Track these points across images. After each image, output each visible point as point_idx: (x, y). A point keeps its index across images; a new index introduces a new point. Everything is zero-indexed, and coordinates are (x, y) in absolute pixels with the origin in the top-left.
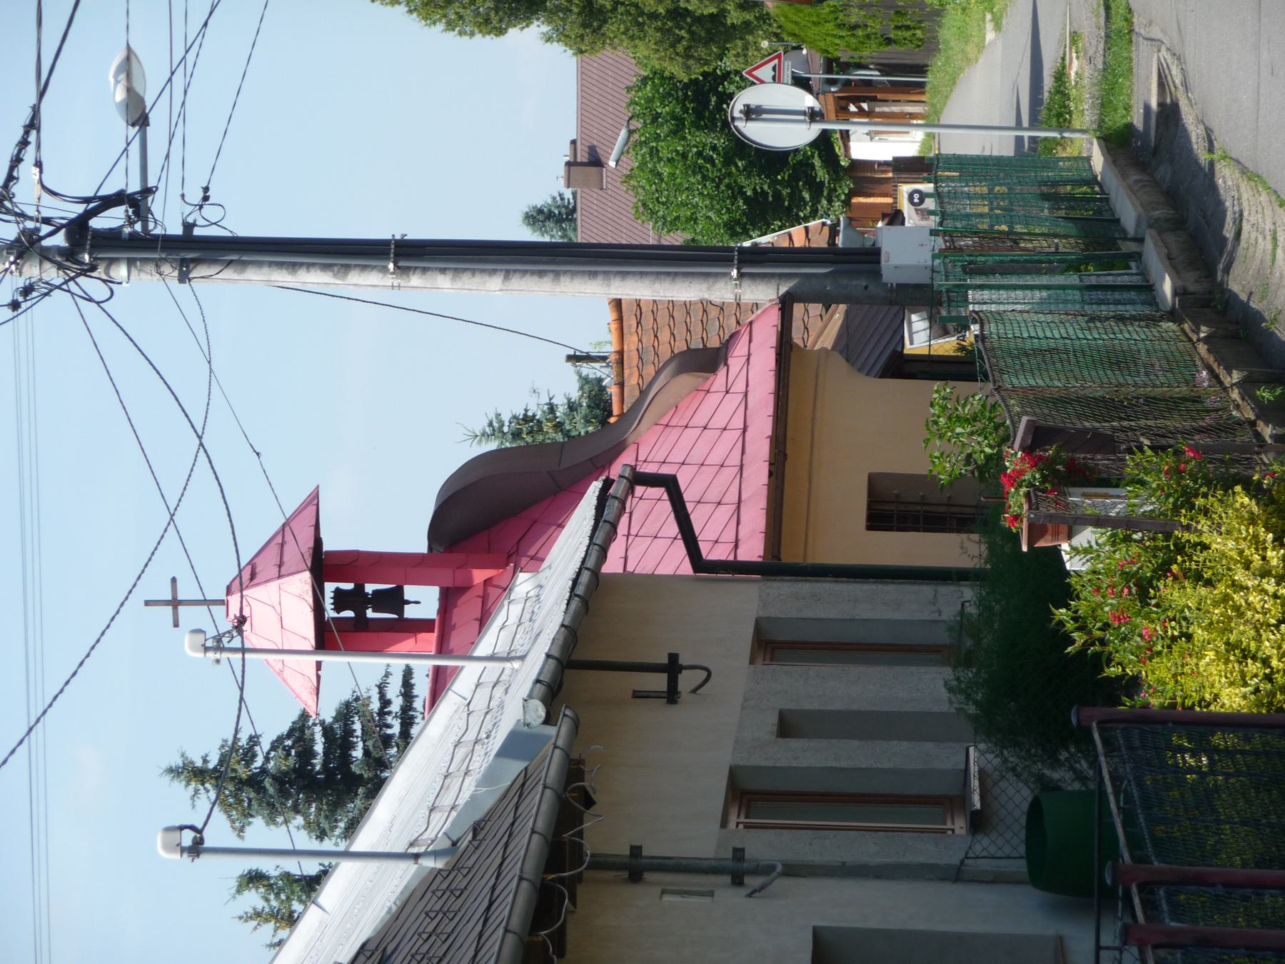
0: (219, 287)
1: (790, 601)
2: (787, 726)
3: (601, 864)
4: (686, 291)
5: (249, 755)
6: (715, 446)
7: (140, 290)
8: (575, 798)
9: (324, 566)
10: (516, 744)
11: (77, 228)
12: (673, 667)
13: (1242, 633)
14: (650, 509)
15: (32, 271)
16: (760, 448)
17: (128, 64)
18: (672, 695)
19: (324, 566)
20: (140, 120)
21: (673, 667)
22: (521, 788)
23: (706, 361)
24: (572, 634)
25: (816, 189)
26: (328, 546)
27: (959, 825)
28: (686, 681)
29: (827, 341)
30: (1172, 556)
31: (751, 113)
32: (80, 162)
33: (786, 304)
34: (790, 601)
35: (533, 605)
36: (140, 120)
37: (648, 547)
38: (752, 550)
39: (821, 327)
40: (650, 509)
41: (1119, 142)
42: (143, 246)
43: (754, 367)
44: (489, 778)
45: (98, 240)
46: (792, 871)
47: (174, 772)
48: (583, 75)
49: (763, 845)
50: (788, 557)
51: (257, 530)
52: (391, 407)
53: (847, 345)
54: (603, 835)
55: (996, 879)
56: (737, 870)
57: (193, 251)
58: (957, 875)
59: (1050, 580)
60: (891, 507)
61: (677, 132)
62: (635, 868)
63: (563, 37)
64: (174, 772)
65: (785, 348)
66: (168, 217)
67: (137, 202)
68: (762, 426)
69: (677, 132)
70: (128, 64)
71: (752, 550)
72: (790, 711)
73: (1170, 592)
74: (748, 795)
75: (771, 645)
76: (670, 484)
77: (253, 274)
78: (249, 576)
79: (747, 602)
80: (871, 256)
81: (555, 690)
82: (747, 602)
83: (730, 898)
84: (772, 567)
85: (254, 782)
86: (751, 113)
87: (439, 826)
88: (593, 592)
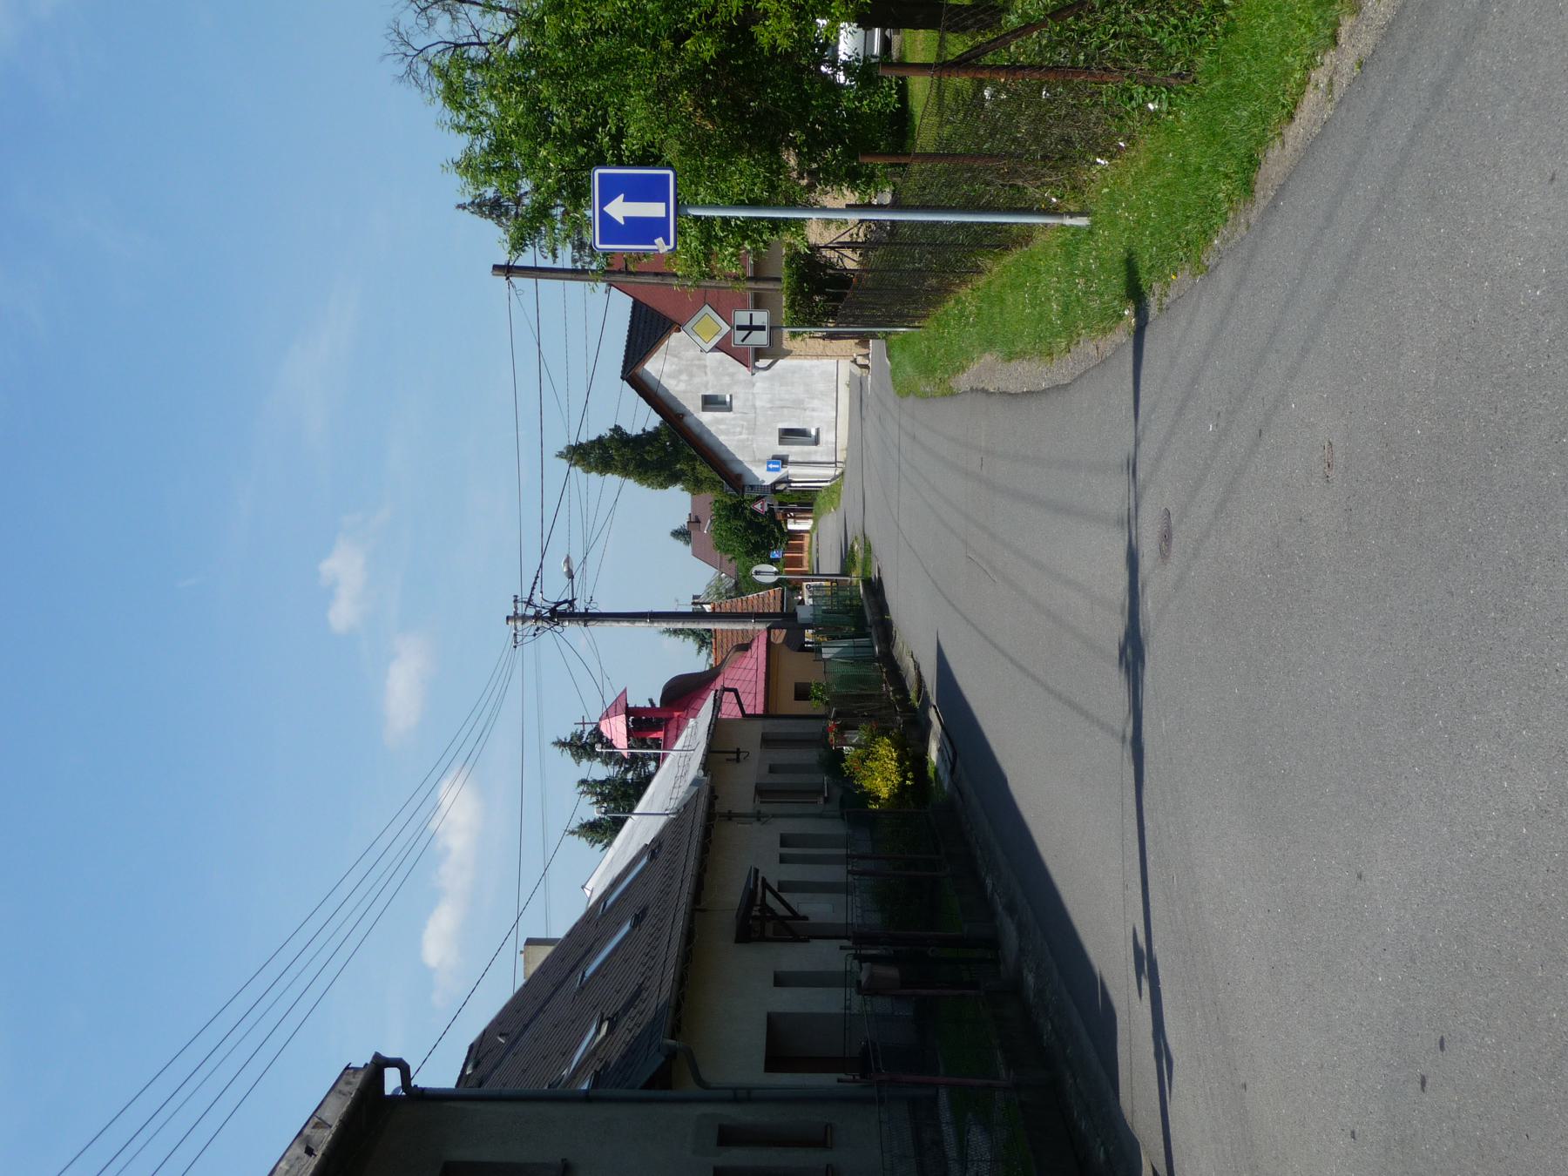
0: (596, 628)
1: (773, 727)
2: (773, 769)
3: (722, 815)
4: (738, 627)
5: (580, 737)
6: (747, 677)
7: (572, 629)
8: (713, 797)
9: (629, 712)
10: (695, 782)
11: (553, 611)
12: (738, 752)
13: (887, 774)
14: (729, 698)
15: (539, 624)
16: (762, 676)
17: (568, 560)
18: (738, 760)
19: (629, 712)
20: (571, 576)
21: (738, 752)
22: (697, 795)
23: (744, 648)
24: (710, 751)
25: (776, 540)
26: (631, 705)
27: (821, 801)
28: (742, 756)
29: (780, 641)
30: (868, 755)
31: (757, 573)
32: (554, 591)
33: (769, 630)
34: (773, 727)
35: (694, 734)
36: (571, 576)
37: (730, 710)
38: (760, 710)
39: (779, 636)
40: (729, 698)
41: (868, 583)
42: (572, 616)
43: (759, 650)
44: (688, 792)
45: (560, 614)
46: (774, 816)
47: (555, 744)
48: (693, 502)
49: (765, 809)
50: (772, 712)
51: (609, 701)
52: (652, 663)
53: (787, 641)
54: (721, 807)
55: (833, 817)
56: (758, 816)
57: (588, 617)
58: (820, 816)
59: (840, 756)
60: (802, 693)
61: (728, 521)
62: (730, 816)
63: (688, 489)
64: (555, 744)
65: (769, 643)
66: (580, 607)
67: (571, 603)
68: (762, 669)
69: (728, 521)
70: (568, 560)
71: (760, 710)
72: (780, 1015)
73: (868, 763)
74: (762, 792)
75: (768, 741)
76: (735, 691)
77: (607, 624)
78: (607, 715)
79: (758, 728)
80: (795, 615)
81: (706, 765)
82: (758, 728)
83: (757, 825)
84: (767, 715)
85: (583, 747)
86: (757, 573)
87: (673, 804)
88: (717, 728)
